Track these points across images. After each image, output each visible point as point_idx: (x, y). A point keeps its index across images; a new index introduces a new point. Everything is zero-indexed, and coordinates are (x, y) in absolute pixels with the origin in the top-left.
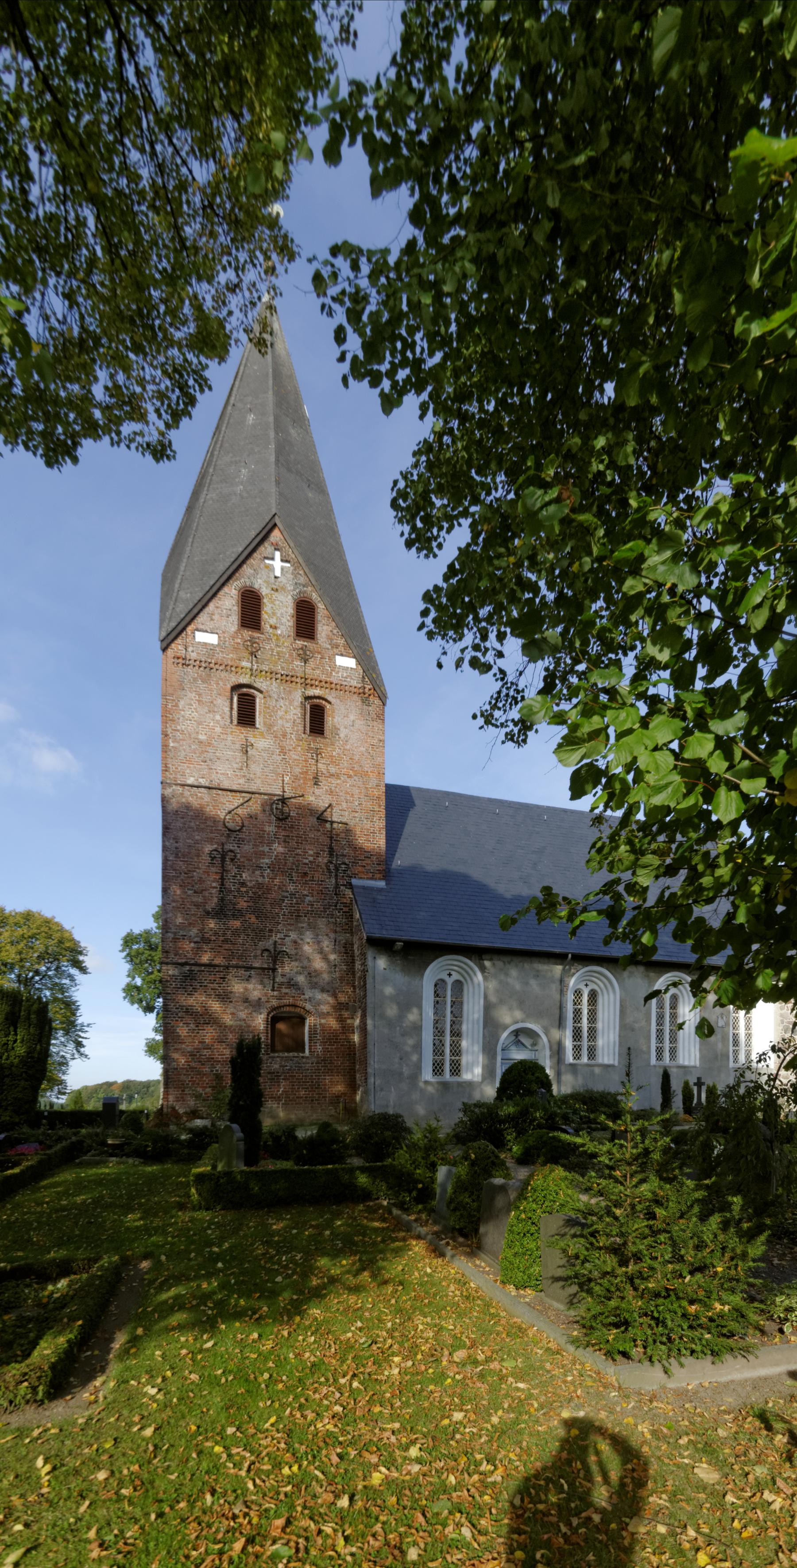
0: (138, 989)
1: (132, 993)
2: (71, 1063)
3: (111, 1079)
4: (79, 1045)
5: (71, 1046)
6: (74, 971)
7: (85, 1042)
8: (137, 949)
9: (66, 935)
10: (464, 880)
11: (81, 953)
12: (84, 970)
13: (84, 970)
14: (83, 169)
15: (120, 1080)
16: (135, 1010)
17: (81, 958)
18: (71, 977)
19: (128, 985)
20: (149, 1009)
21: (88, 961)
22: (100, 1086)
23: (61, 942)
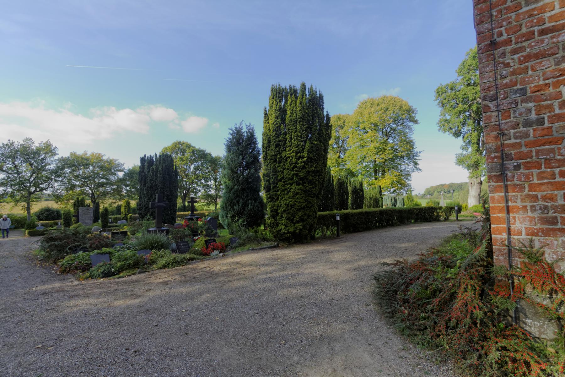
0: (448, 121)
1: (445, 125)
2: (412, 174)
3: (443, 183)
4: (416, 164)
5: (412, 165)
6: (411, 124)
7: (419, 162)
8: (446, 96)
9: (403, 103)
10: (452, 183)
11: (413, 112)
12: (416, 122)
13: (416, 122)
14: (468, 368)
15: (447, 183)
16: (448, 137)
17: (413, 115)
18: (409, 128)
19: (440, 120)
20: (457, 134)
21: (417, 117)
22: (439, 186)
23: (401, 107)
